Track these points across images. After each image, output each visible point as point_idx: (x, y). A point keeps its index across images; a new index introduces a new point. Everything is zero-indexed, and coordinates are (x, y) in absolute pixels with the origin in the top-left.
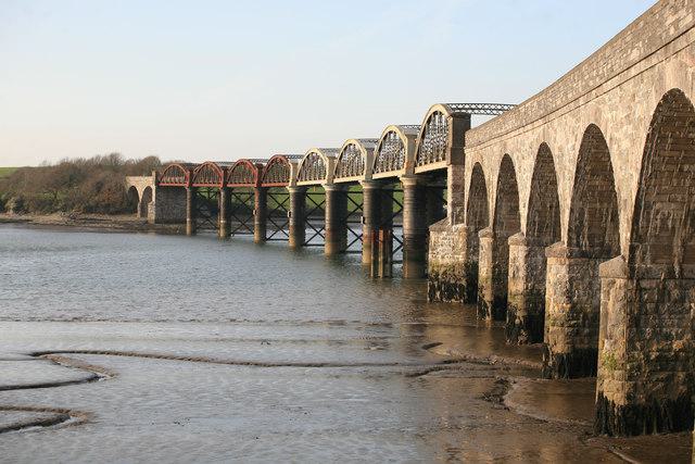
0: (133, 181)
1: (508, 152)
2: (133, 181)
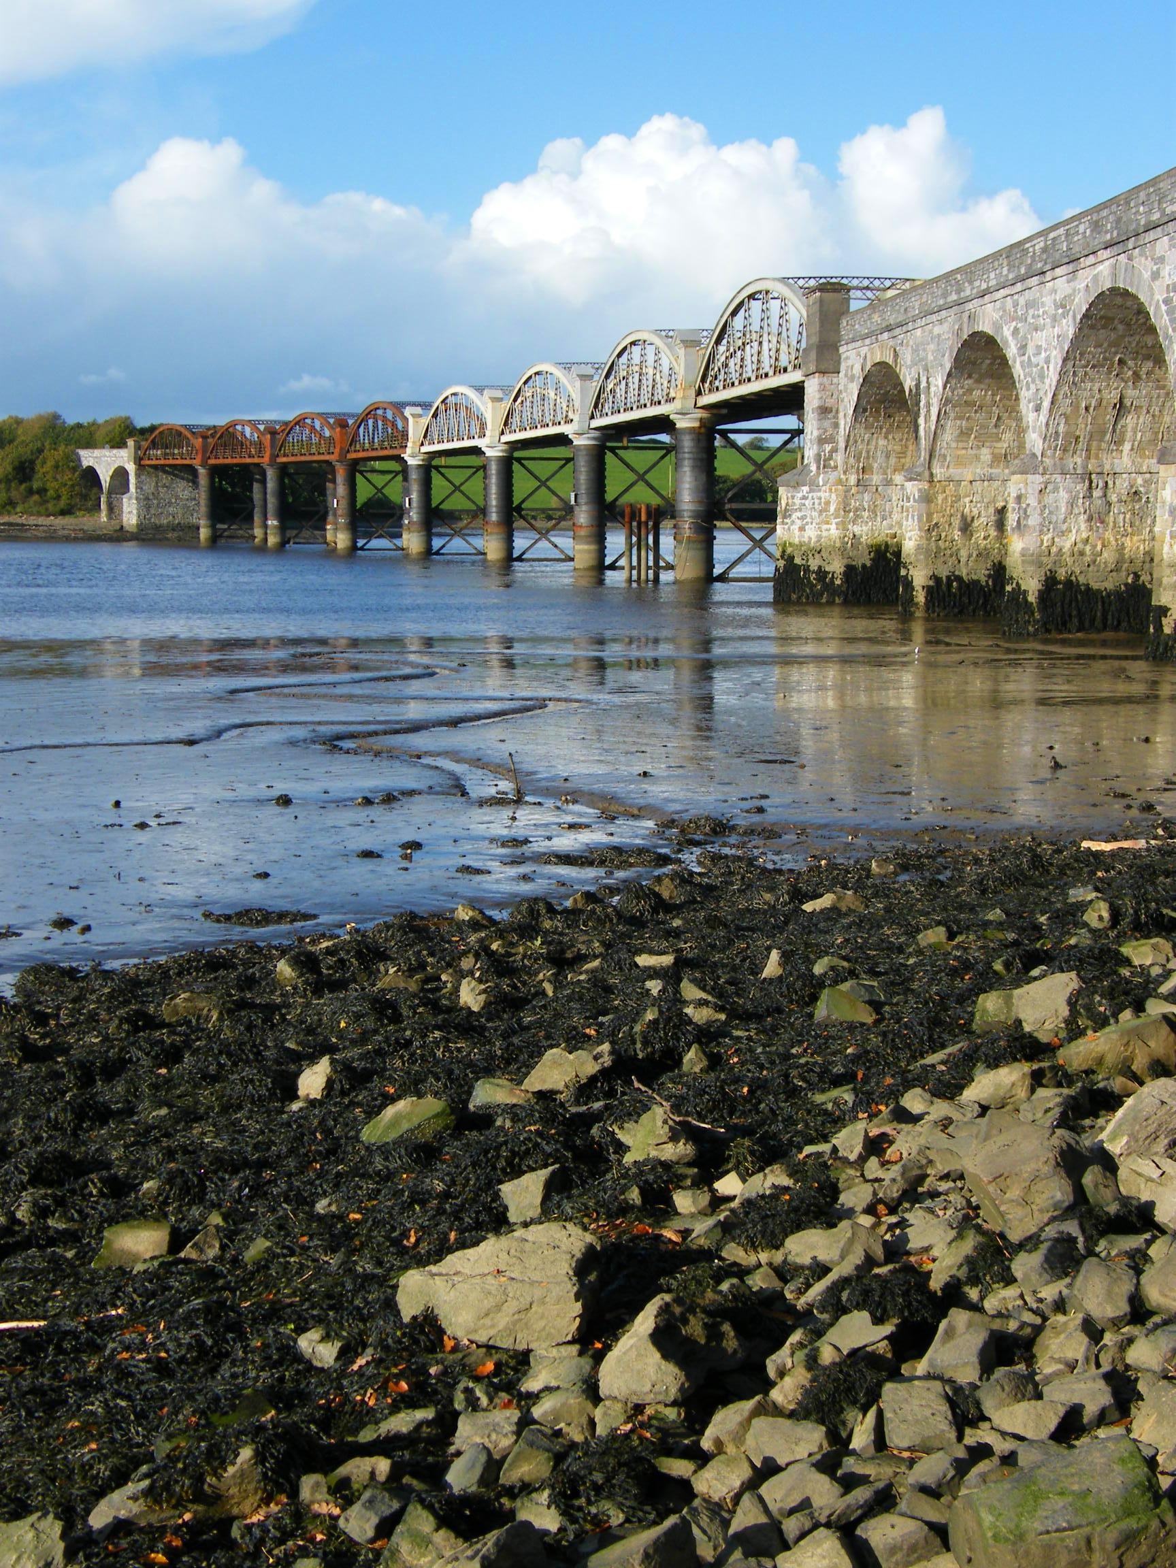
0: (88, 458)
1: (985, 327)
2: (88, 458)
